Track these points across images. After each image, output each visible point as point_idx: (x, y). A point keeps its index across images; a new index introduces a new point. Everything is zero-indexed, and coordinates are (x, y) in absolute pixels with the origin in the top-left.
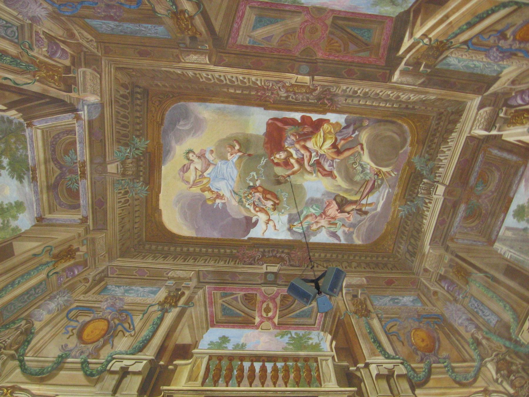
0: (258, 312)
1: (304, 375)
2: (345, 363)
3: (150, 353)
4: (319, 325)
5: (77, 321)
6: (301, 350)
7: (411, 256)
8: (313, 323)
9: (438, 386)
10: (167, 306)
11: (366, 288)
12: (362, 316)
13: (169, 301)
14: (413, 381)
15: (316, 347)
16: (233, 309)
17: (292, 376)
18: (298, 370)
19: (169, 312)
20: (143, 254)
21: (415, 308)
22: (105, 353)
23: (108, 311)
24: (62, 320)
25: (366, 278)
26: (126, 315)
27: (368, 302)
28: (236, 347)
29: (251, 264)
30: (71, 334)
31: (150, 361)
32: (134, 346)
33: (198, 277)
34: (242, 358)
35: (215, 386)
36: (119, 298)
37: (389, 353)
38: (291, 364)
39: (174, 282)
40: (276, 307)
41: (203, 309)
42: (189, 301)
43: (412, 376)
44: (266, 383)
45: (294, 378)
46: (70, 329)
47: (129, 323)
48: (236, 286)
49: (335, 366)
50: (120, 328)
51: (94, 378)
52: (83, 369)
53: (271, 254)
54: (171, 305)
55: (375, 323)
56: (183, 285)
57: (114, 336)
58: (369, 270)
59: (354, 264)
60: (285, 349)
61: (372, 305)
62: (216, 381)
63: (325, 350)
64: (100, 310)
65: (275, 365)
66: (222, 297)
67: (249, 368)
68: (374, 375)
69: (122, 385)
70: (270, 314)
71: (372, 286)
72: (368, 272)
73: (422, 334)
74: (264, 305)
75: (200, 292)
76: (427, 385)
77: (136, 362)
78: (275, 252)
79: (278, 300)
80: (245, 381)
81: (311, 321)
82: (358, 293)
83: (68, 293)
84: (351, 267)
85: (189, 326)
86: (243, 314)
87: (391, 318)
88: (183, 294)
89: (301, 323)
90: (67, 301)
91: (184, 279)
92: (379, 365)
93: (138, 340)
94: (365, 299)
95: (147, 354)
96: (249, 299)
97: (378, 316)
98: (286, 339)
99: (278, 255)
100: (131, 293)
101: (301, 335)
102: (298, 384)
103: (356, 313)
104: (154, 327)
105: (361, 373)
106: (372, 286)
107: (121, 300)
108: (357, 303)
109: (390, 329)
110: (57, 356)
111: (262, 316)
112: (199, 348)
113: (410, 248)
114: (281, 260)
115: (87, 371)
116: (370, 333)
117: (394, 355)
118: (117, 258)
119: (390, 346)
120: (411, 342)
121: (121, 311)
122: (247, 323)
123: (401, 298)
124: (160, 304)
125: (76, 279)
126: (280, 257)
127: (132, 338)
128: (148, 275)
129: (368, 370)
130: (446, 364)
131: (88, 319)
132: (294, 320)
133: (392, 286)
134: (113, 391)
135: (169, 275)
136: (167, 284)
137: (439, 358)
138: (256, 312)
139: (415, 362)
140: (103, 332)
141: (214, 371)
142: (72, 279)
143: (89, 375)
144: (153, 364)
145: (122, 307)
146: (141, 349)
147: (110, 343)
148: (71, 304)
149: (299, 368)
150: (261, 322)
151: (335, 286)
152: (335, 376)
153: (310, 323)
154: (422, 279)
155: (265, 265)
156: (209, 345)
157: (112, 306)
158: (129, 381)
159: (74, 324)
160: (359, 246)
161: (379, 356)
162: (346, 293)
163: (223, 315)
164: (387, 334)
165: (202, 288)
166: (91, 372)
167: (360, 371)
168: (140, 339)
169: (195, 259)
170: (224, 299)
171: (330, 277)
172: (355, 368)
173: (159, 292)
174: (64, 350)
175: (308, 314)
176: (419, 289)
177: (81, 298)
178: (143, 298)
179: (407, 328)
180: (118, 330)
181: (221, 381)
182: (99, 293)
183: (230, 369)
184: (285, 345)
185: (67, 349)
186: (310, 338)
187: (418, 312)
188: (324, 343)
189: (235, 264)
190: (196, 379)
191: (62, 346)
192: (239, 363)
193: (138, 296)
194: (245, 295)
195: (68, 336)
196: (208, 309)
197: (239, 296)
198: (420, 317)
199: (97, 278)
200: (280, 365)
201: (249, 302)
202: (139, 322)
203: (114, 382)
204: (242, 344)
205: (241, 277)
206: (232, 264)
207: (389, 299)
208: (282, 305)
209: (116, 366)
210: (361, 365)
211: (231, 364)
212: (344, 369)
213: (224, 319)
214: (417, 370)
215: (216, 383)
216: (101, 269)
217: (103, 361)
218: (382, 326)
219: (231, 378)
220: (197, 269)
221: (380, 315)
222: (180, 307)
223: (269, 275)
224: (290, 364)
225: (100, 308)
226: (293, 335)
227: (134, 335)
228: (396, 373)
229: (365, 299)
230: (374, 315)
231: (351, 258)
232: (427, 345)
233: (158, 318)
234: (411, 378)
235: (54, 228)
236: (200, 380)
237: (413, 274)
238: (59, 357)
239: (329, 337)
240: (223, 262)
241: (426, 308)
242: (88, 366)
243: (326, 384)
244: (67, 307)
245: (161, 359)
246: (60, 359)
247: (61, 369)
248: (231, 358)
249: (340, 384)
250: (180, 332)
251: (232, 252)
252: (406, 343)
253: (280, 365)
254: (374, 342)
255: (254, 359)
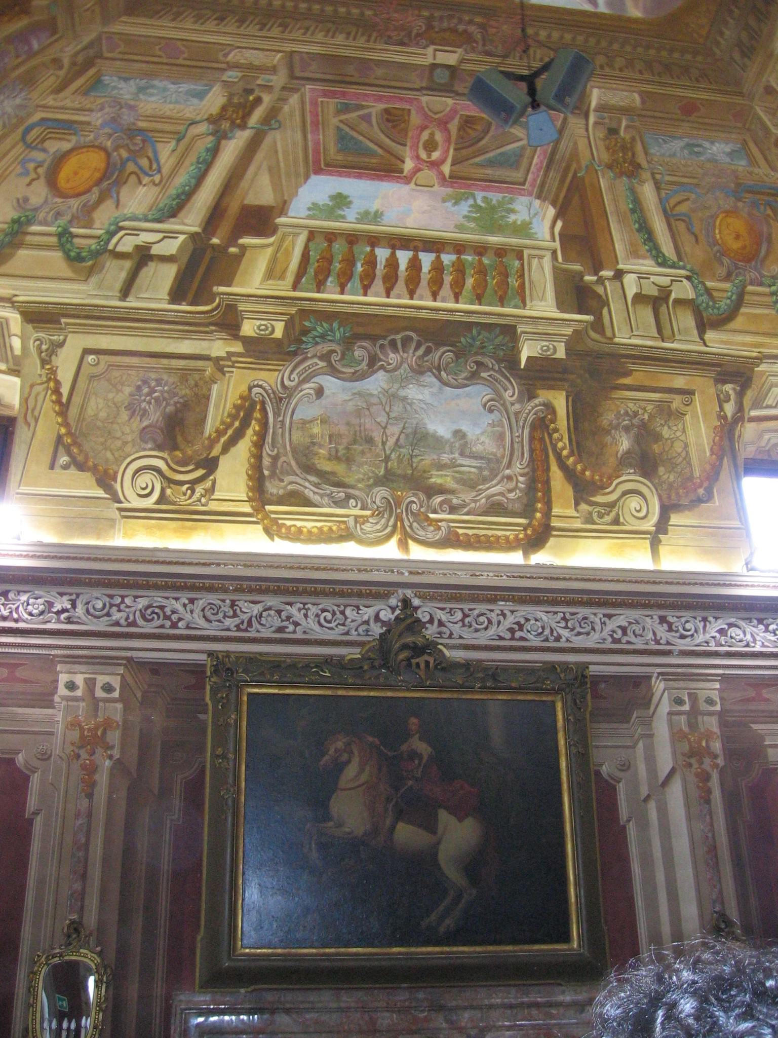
0: (411, 148)
1: (492, 282)
2: (577, 267)
3: (192, 221)
4: (533, 185)
5: (44, 150)
6: (492, 233)
7: (744, 55)
8: (522, 180)
9: (753, 328)
10: (225, 125)
11: (639, 115)
12: (622, 174)
13: (229, 113)
14: (704, 315)
15: (523, 230)
16: (361, 138)
17: (470, 282)
18: (482, 272)
19: (230, 139)
20: (175, 10)
21: (733, 167)
22: (104, 216)
23: (107, 130)
24: (13, 147)
25: (641, 94)
26: (144, 141)
27: (639, 148)
28: (365, 216)
29: (402, 44)
30: (34, 176)
31: (193, 236)
32: (161, 205)
33: (291, 68)
34: (374, 240)
35: (318, 292)
36: (126, 104)
37: (667, 255)
38: (469, 258)
39: (240, 74)
40: (448, 140)
41: (299, 136)
42: (271, 118)
43: (704, 305)
44: (419, 292)
45: (474, 288)
46: (31, 166)
47: (148, 158)
48: (368, 91)
49: (556, 270)
50: (131, 167)
51: (83, 264)
52: (61, 246)
53: (445, 25)
54: (233, 122)
55: (648, 192)
56: (259, 82)
57: (120, 183)
58: (651, 77)
59: (619, 62)
60: (460, 228)
61: (646, 153)
62: (320, 281)
63: (539, 236)
64: (89, 128)
65: (438, 258)
66: (339, 112)
67: (387, 260)
68: (630, 294)
69: (138, 281)
70: (435, 155)
71: (649, 113)
72: (648, 82)
73: (738, 224)
74: (425, 135)
75: (294, 99)
76: (732, 325)
77: (165, 237)
78: (455, 21)
79: (453, 126)
80: (378, 285)
81: (518, 175)
82: (620, 126)
83: (22, 90)
84: (611, 66)
85: (270, 169)
86: (380, 151)
87: (682, 184)
88: (258, 100)
89: (496, 178)
90: (20, 107)
91: (261, 69)
92: (642, 276)
93: (167, 194)
94: (633, 139)
95: (186, 221)
96: (394, 121)
97: (654, 178)
98: (464, 208)
99: (461, 28)
100: (152, 95)
101: (494, 202)
102: (479, 299)
103: (610, 167)
104: (200, 168)
105: (605, 289)
106: (649, 113)
107: (131, 108)
108: (616, 145)
109: (674, 206)
110: (9, 220)
111: (418, 157)
112: (291, 214)
113: (744, 35)
114: (465, 40)
115: (70, 250)
116: (633, 211)
117: (675, 259)
118: (120, 17)
119: (667, 232)
120: (714, 237)
121: (132, 132)
122: (388, 170)
123: (707, 144)
124: (212, 120)
125: (33, 62)
126: (465, 31)
127: (156, 190)
128: (186, 55)
129: (619, 284)
130: (774, 288)
131: (66, 146)
132: (482, 171)
133: (692, 118)
134: (121, 291)
135: (230, 58)
136: (225, 78)
137: (762, 276)
138: (408, 148)
139: (713, 277)
140: (97, 175)
141: (318, 261)
142: (28, 59)
143: (75, 259)
144: (198, 246)
145: (134, 124)
146: (174, 212)
147: (112, 197)
148: (30, 115)
149: (485, 267)
150: (417, 170)
151: (569, 94)
152: (553, 294)
153: (515, 180)
154: (757, 108)
155: (430, 49)
156: (309, 209)
157: (114, 120)
158: (151, 273)
159: (39, 156)
160: (636, 21)
161: (644, 258)
162: (596, 123)
163: (339, 151)
164: (668, 216)
165: (295, 90)
166: (79, 254)
167: (603, 284)
168: (173, 191)
169: (284, 26)
170: (343, 117)
171: (558, 74)
172: (595, 278)
173: (210, 95)
174: (23, 208)
175: (513, 161)
176: (749, 130)
177: (50, 101)
178: (178, 106)
179: (708, 208)
180: (128, 172)
181: (331, 282)
182: (86, 91)
183: (350, 262)
184: (462, 220)
185: (29, 207)
186: (513, 211)
187: (737, 177)
188: (538, 221)
189: (368, 41)
190: (282, 277)
191: (18, 200)
192: (368, 249)
193: (165, 102)
194: (387, 111)
195: (28, 180)
196: (309, 136)
197: (374, 111)
198: (740, 190)
199: (80, 59)
200: (448, 259)
201: (394, 127)
202: (169, 158)
203: (123, 275)
204: (377, 212)
205: (379, 72)
206: (361, 41)
207: (682, 144)
208: (462, 138)
209: (127, 244)
210: (607, 273)
211: (351, 251)
212: (574, 277)
213: (339, 158)
214: (715, 294)
215: (320, 286)
216: (86, 40)
217: (100, 232)
218: (660, 199)
219: (350, 278)
220: (289, 47)
221: (658, 177)
222: (252, 128)
223: (439, 71)
224: (468, 258)
225: (89, 123)
226: (479, 202)
227: (161, 181)
228: (673, 296)
229: (633, 139)
230: (646, 175)
231: (616, 46)
232: (744, 247)
233: (208, 150)
234: (701, 308)
235: (45, 554)
236: (290, 277)
237: (741, 94)
238: (14, 221)
239: (551, 212)
240: (343, 36)
241: (756, 170)
242: (71, 242)
243: (534, 302)
244: (21, 120)
245: (213, 234)
246: (16, 226)
247: (20, 245)
248: (352, 239)
249: (561, 306)
250: (253, 180)
251: (362, 14)
252: (702, 238)
253: (448, 259)
254: (639, 230)
255: (398, 244)
